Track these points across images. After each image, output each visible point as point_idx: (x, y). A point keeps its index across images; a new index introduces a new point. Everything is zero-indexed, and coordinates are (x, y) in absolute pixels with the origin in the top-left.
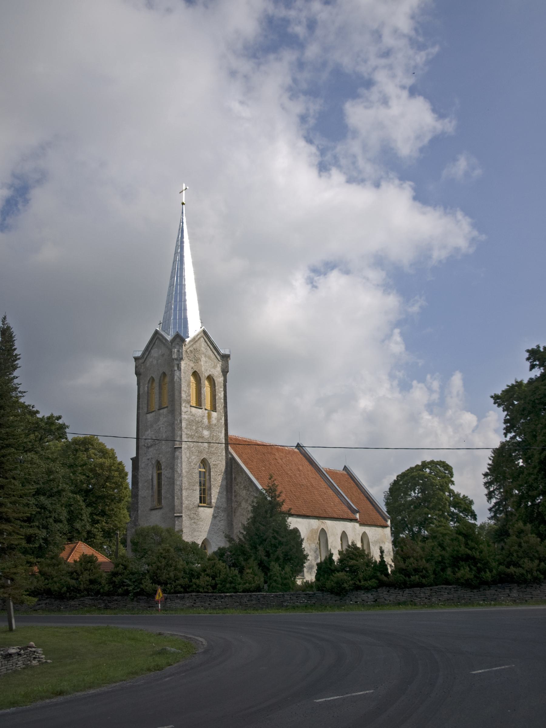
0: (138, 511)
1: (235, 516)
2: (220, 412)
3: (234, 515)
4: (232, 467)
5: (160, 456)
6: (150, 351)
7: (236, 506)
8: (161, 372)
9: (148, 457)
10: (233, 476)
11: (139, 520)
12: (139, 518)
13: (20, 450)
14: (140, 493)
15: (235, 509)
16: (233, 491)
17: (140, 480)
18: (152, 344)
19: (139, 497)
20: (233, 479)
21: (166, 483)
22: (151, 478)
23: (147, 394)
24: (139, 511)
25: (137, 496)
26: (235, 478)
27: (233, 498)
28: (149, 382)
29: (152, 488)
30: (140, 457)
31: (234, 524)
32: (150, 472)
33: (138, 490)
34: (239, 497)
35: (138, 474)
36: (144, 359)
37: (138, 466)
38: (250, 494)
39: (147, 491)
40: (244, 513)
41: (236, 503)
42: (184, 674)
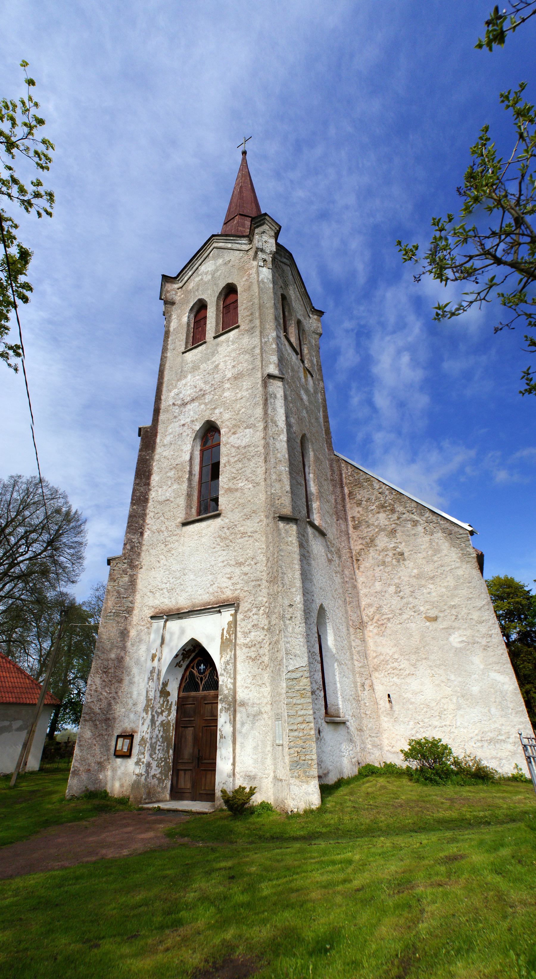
0: (142, 534)
1: (359, 569)
2: (392, 565)
3: (356, 566)
4: (341, 475)
5: (217, 411)
6: (198, 268)
7: (361, 547)
8: (222, 284)
9: (182, 422)
10: (346, 491)
11: (143, 554)
12: (144, 548)
13: (314, 858)
14: (152, 495)
15: (359, 554)
16: (349, 519)
17: (159, 431)
18: (202, 259)
19: (150, 504)
20: (347, 497)
21: (232, 460)
22: (187, 458)
23: (186, 326)
24: (146, 535)
25: (146, 500)
26: (350, 493)
27: (350, 532)
28: (191, 310)
29: (190, 480)
30: (161, 428)
31: (360, 586)
32: (187, 448)
33: (150, 490)
34: (368, 526)
35: (152, 458)
36: (184, 282)
37: (155, 442)
38: (399, 518)
39: (175, 486)
40: (388, 559)
41: (360, 541)
42: (168, 872)
